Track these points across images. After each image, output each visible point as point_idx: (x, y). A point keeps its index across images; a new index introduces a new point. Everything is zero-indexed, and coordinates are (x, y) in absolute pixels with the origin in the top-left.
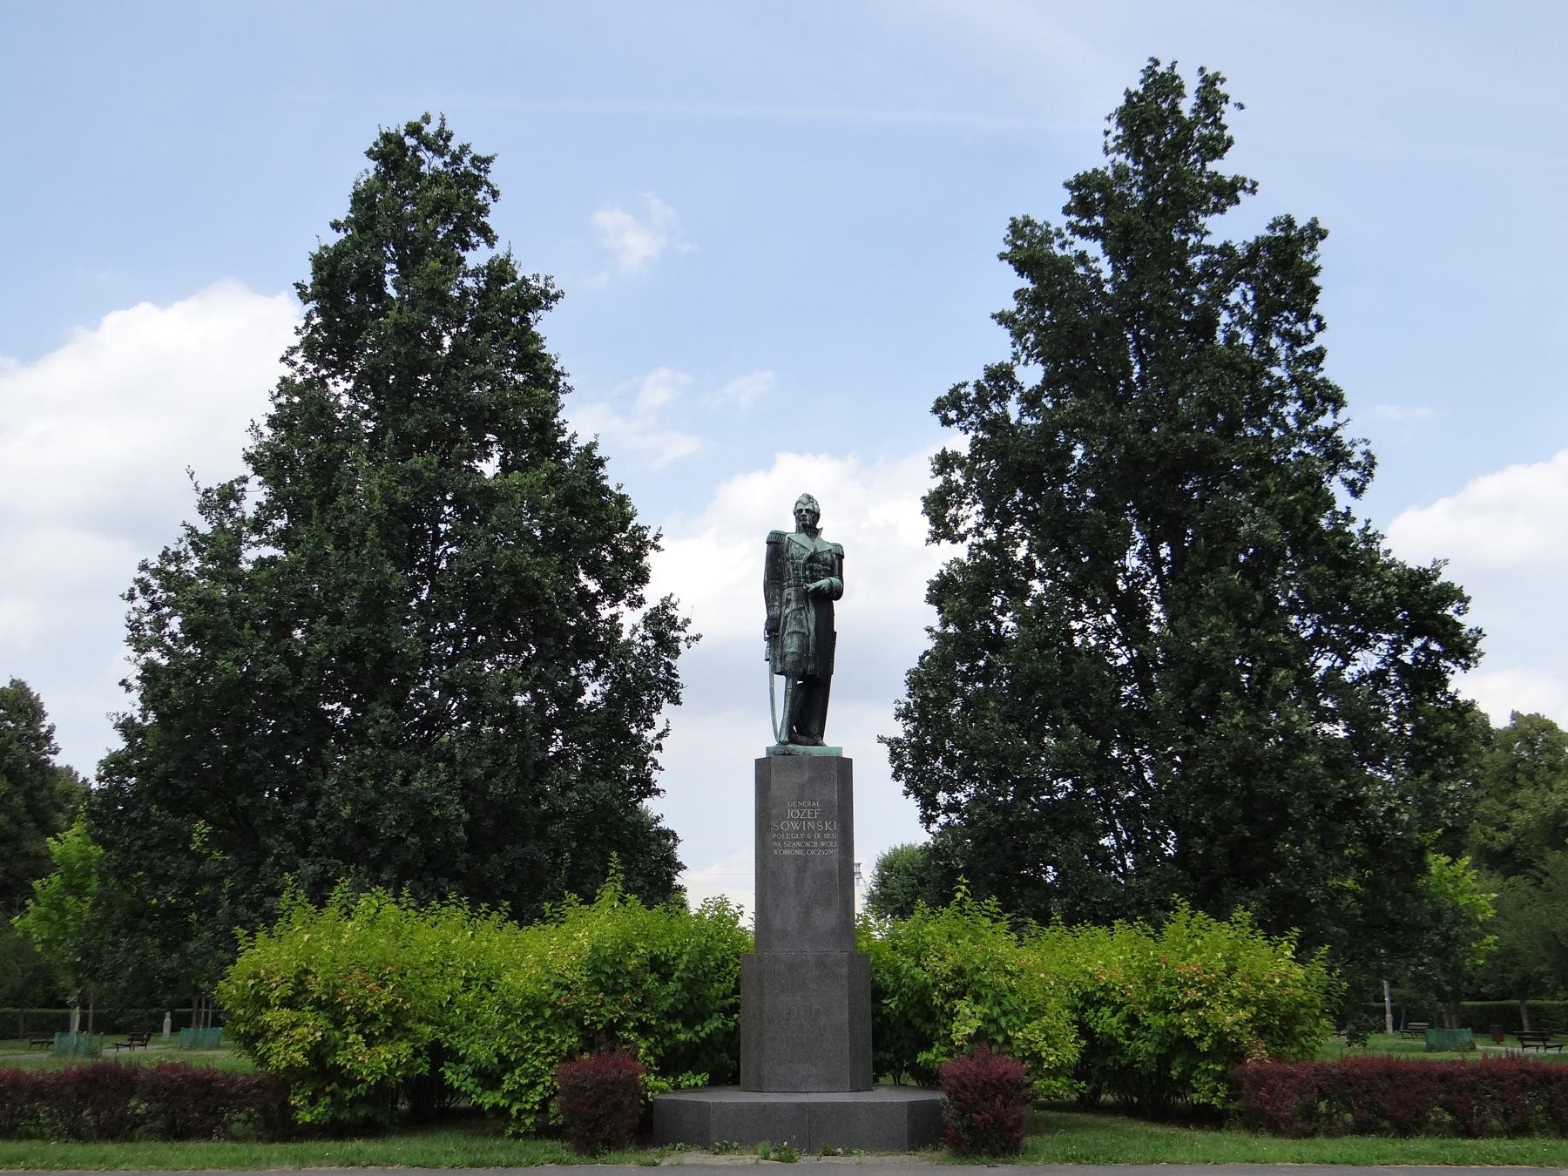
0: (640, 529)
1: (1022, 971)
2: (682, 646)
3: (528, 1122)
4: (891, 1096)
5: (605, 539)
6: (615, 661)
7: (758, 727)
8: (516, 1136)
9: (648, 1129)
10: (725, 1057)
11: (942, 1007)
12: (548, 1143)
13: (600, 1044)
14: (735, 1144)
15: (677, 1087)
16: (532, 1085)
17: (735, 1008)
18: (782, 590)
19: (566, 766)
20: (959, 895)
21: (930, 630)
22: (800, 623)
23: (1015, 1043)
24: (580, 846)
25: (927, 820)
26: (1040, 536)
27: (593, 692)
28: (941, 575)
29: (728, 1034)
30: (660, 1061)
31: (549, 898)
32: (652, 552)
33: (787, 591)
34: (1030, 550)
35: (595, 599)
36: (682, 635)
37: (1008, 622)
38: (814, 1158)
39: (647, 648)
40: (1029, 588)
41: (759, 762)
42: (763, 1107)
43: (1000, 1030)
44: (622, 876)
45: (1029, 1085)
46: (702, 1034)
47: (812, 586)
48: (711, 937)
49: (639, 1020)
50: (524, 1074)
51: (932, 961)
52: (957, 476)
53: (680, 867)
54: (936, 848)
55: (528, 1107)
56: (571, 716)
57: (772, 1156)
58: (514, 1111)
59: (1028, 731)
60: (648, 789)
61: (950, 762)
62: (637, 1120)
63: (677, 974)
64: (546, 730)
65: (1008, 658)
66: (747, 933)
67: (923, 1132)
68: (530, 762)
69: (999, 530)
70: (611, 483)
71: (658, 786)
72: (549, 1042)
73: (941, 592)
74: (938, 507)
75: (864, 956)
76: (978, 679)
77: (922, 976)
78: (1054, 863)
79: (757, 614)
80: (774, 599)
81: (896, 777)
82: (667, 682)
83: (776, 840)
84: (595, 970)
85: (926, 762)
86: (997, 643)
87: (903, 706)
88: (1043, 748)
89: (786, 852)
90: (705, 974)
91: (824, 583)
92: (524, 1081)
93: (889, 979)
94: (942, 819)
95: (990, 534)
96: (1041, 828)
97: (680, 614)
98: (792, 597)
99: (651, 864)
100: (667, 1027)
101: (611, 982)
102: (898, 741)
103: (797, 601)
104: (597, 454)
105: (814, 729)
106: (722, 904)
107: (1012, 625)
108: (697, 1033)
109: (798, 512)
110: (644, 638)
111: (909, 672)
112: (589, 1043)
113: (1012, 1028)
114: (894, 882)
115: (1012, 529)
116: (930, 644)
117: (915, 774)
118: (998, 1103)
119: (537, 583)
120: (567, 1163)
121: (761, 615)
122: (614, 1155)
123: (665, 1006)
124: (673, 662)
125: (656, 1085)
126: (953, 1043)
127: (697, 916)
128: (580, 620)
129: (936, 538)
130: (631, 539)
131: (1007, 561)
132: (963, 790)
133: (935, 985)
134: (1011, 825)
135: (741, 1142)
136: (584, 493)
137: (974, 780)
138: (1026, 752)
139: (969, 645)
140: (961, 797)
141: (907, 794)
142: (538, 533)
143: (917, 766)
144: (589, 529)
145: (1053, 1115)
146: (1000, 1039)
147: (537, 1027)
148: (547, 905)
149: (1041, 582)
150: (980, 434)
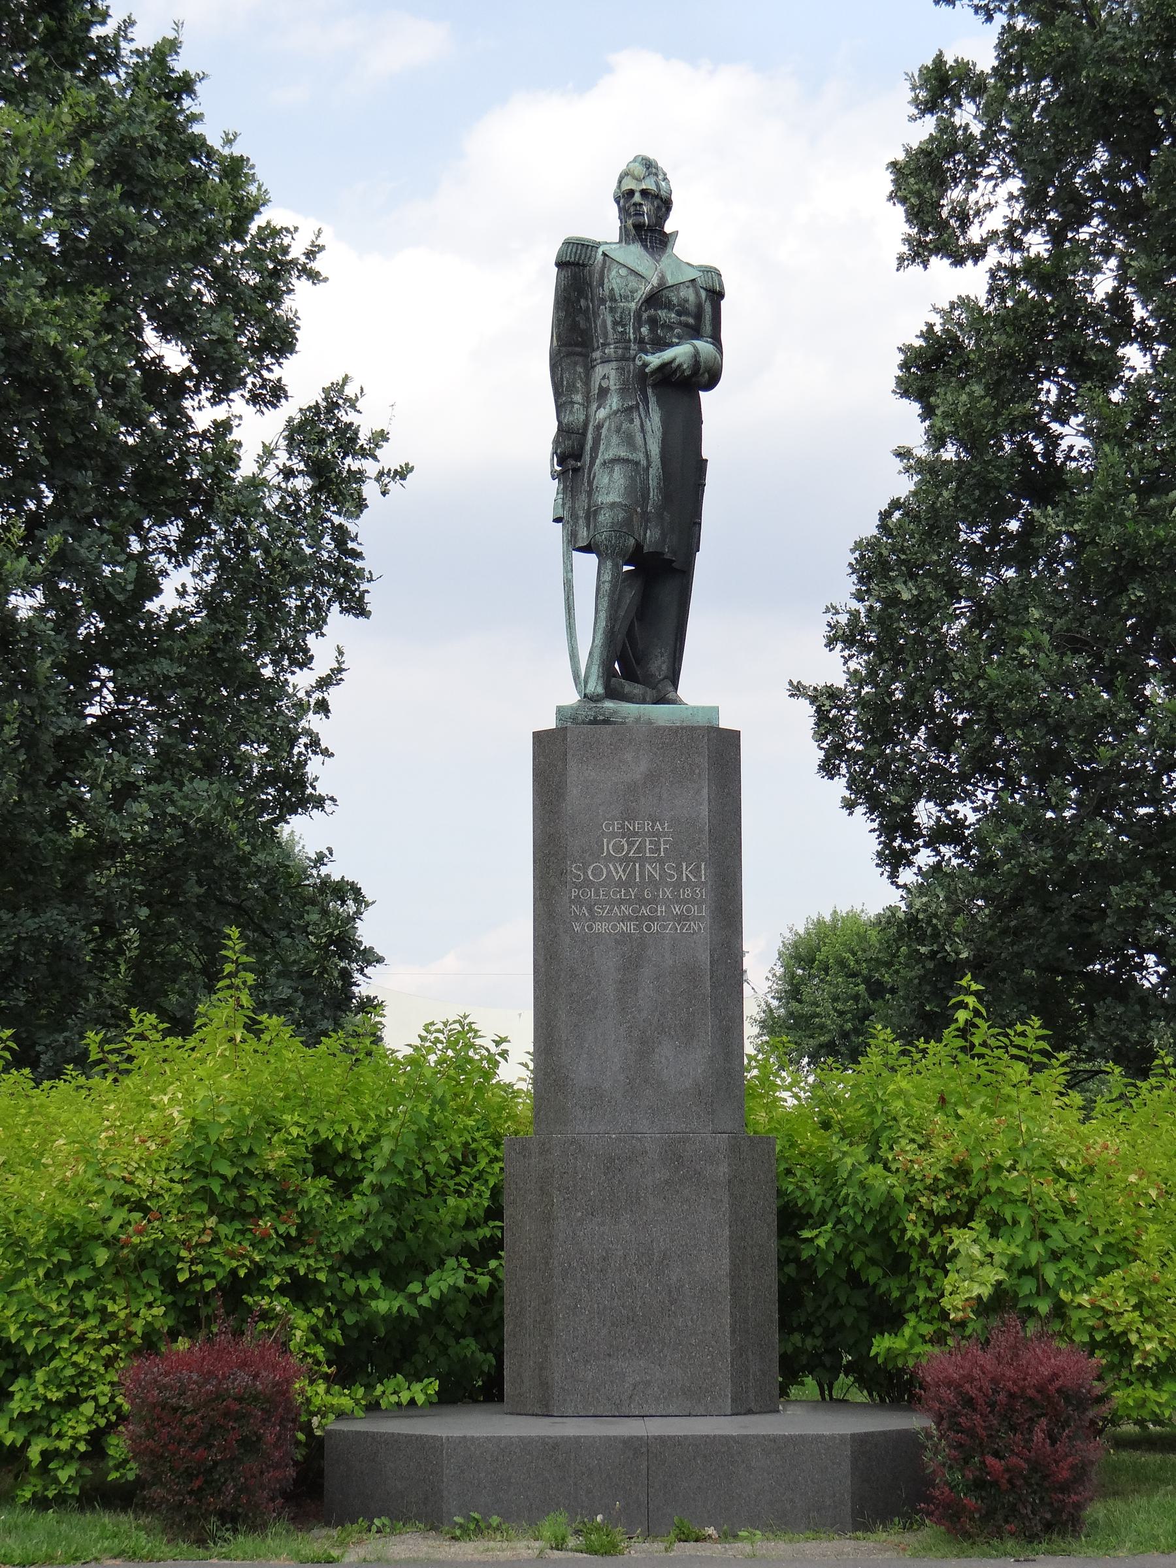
0: (276, 233)
1: (1090, 1170)
2: (370, 490)
3: (63, 1475)
4: (824, 1423)
5: (199, 255)
6: (227, 523)
7: (543, 668)
8: (40, 1503)
9: (315, 1489)
10: (470, 1346)
11: (924, 1244)
12: (107, 1519)
13: (210, 1320)
14: (495, 1520)
15: (373, 1407)
16: (72, 1402)
17: (493, 1247)
18: (589, 368)
19: (123, 745)
20: (962, 1016)
21: (903, 454)
22: (629, 441)
23: (1075, 1315)
24: (157, 916)
25: (893, 860)
26: (1146, 247)
27: (178, 589)
28: (929, 333)
29: (475, 1300)
30: (337, 1354)
31: (101, 1022)
32: (301, 285)
33: (600, 370)
34: (1122, 278)
35: (178, 386)
36: (370, 468)
37: (1072, 437)
38: (658, 1546)
39: (295, 495)
40: (1119, 363)
41: (540, 738)
42: (552, 1446)
43: (1044, 1289)
44: (250, 978)
45: (1101, 1399)
46: (424, 1301)
47: (655, 360)
48: (442, 1103)
49: (291, 1271)
50: (54, 1380)
51: (905, 1152)
52: (968, 116)
53: (370, 958)
54: (912, 920)
55: (64, 1445)
56: (130, 635)
57: (572, 1542)
58: (34, 1454)
59: (1112, 670)
60: (297, 794)
61: (942, 739)
62: (291, 1472)
63: (370, 1178)
64: (78, 670)
65: (1073, 514)
66: (516, 1094)
67: (886, 1492)
68: (46, 739)
69: (1057, 236)
70: (210, 131)
71: (322, 789)
72: (105, 1316)
73: (929, 369)
74: (924, 182)
75: (763, 1143)
76: (1006, 559)
77: (881, 1182)
78: (1160, 949)
79: (532, 421)
80: (572, 388)
81: (828, 769)
82: (339, 568)
83: (577, 901)
84: (201, 1170)
85: (891, 737)
86: (1047, 482)
87: (843, 619)
88: (1143, 706)
90: (429, 1180)
91: (680, 352)
92: (55, 1395)
93: (813, 1188)
94: (924, 858)
95: (1037, 244)
96: (1134, 875)
97: (365, 422)
98: (613, 383)
99: (309, 953)
100: (349, 1287)
101: (233, 1194)
102: (832, 694)
103: (623, 391)
104: (179, 65)
105: (659, 665)
106: (462, 1035)
107: (1081, 443)
108: (413, 1298)
109: (624, 198)
110: (288, 473)
111: (858, 545)
112: (189, 1320)
113: (1070, 1285)
114: (817, 992)
115: (1084, 234)
116: (904, 486)
117: (869, 763)
118: (1039, 1435)
119: (56, 354)
120: (150, 1558)
122: (245, 1542)
123: (346, 1242)
124: (351, 526)
125: (329, 1405)
126: (944, 1315)
127: (411, 1060)
128: (149, 431)
129: (919, 253)
130: (255, 256)
131: (1074, 307)
132: (970, 796)
133: (910, 1200)
134: (1072, 872)
135: (506, 1517)
136: (153, 152)
137: (993, 775)
138: (1104, 717)
139: (988, 486)
140: (965, 810)
141: (849, 806)
142: (52, 241)
143: (877, 746)
144: (164, 233)
145: (1153, 1459)
146: (1044, 1307)
147: (77, 1286)
148: (93, 1038)
149: (1145, 349)
150: (1020, 22)
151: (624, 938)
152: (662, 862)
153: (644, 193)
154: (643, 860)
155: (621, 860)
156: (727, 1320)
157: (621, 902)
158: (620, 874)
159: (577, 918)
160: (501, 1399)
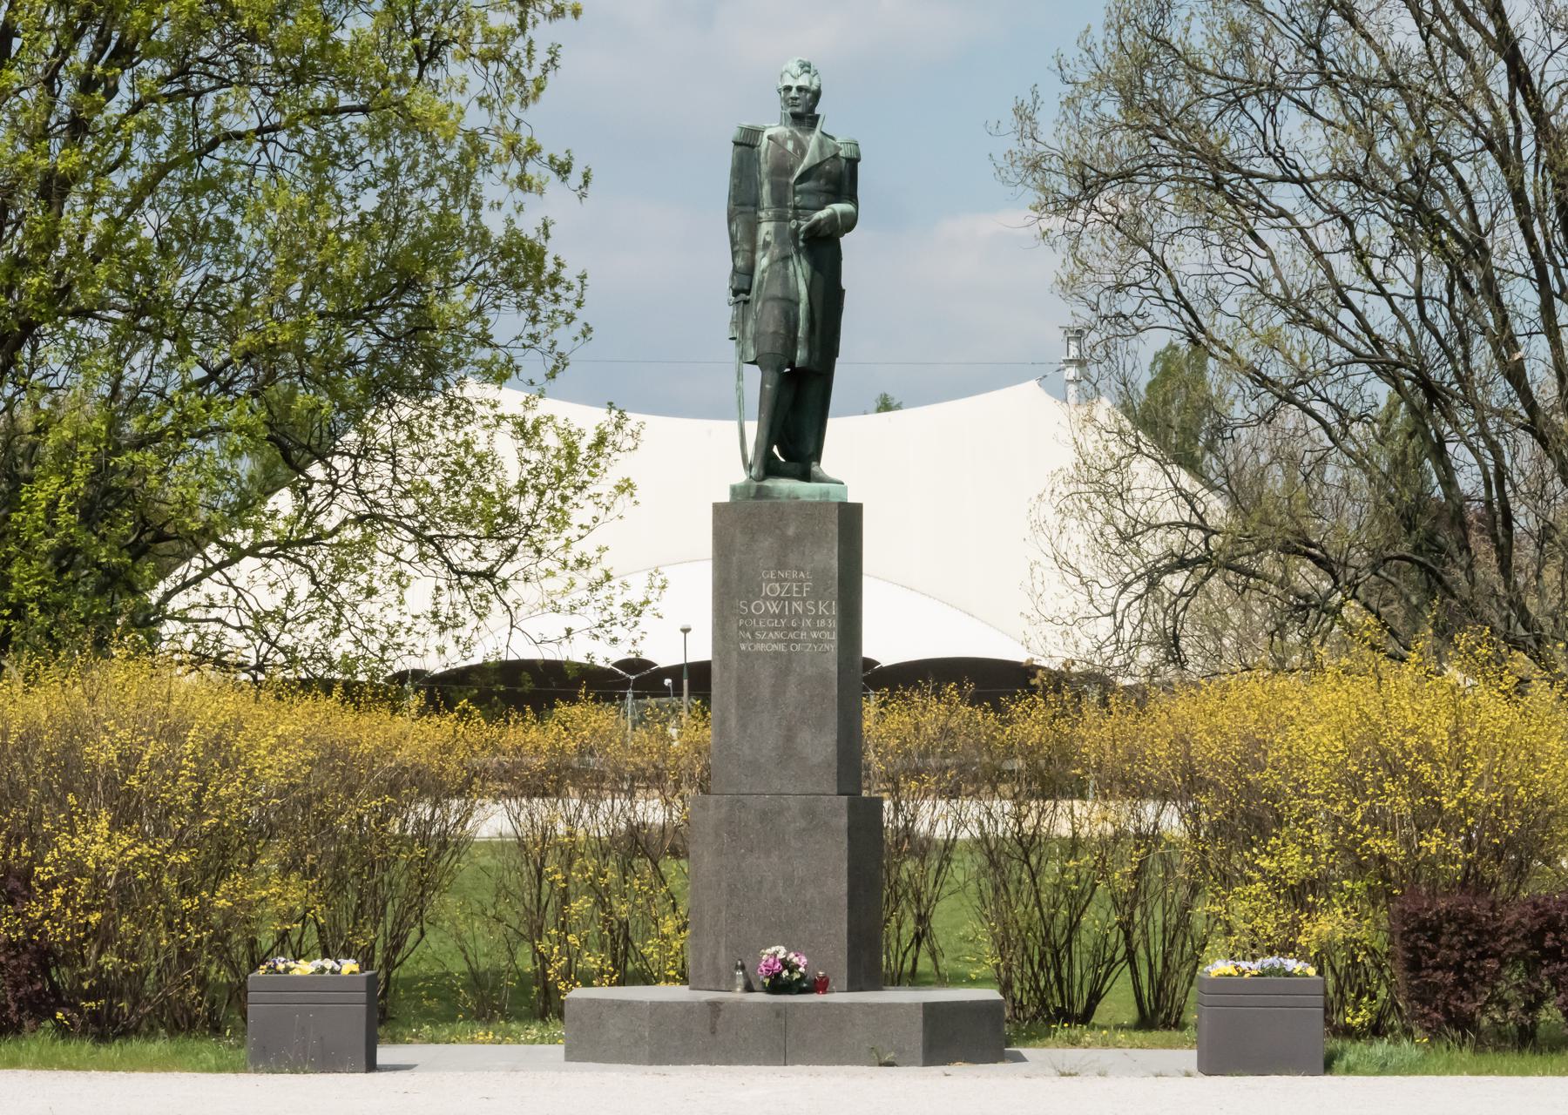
41: (718, 509)
83: (743, 628)
89: (760, 647)
121: (721, 265)
151: (777, 654)
152: (804, 600)
153: (800, 89)
154: (790, 599)
155: (775, 599)
156: (845, 926)
157: (774, 629)
158: (774, 608)
159: (743, 640)
160: (1179, 1025)
